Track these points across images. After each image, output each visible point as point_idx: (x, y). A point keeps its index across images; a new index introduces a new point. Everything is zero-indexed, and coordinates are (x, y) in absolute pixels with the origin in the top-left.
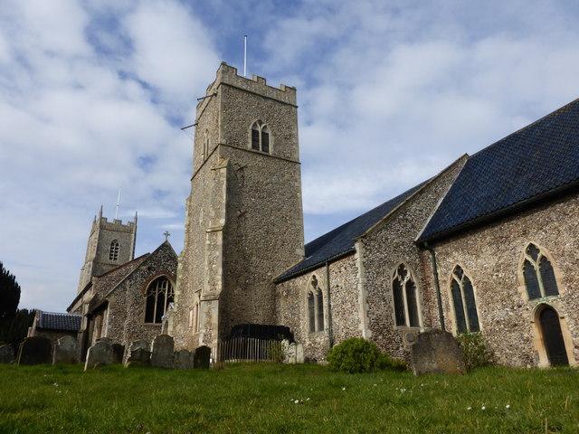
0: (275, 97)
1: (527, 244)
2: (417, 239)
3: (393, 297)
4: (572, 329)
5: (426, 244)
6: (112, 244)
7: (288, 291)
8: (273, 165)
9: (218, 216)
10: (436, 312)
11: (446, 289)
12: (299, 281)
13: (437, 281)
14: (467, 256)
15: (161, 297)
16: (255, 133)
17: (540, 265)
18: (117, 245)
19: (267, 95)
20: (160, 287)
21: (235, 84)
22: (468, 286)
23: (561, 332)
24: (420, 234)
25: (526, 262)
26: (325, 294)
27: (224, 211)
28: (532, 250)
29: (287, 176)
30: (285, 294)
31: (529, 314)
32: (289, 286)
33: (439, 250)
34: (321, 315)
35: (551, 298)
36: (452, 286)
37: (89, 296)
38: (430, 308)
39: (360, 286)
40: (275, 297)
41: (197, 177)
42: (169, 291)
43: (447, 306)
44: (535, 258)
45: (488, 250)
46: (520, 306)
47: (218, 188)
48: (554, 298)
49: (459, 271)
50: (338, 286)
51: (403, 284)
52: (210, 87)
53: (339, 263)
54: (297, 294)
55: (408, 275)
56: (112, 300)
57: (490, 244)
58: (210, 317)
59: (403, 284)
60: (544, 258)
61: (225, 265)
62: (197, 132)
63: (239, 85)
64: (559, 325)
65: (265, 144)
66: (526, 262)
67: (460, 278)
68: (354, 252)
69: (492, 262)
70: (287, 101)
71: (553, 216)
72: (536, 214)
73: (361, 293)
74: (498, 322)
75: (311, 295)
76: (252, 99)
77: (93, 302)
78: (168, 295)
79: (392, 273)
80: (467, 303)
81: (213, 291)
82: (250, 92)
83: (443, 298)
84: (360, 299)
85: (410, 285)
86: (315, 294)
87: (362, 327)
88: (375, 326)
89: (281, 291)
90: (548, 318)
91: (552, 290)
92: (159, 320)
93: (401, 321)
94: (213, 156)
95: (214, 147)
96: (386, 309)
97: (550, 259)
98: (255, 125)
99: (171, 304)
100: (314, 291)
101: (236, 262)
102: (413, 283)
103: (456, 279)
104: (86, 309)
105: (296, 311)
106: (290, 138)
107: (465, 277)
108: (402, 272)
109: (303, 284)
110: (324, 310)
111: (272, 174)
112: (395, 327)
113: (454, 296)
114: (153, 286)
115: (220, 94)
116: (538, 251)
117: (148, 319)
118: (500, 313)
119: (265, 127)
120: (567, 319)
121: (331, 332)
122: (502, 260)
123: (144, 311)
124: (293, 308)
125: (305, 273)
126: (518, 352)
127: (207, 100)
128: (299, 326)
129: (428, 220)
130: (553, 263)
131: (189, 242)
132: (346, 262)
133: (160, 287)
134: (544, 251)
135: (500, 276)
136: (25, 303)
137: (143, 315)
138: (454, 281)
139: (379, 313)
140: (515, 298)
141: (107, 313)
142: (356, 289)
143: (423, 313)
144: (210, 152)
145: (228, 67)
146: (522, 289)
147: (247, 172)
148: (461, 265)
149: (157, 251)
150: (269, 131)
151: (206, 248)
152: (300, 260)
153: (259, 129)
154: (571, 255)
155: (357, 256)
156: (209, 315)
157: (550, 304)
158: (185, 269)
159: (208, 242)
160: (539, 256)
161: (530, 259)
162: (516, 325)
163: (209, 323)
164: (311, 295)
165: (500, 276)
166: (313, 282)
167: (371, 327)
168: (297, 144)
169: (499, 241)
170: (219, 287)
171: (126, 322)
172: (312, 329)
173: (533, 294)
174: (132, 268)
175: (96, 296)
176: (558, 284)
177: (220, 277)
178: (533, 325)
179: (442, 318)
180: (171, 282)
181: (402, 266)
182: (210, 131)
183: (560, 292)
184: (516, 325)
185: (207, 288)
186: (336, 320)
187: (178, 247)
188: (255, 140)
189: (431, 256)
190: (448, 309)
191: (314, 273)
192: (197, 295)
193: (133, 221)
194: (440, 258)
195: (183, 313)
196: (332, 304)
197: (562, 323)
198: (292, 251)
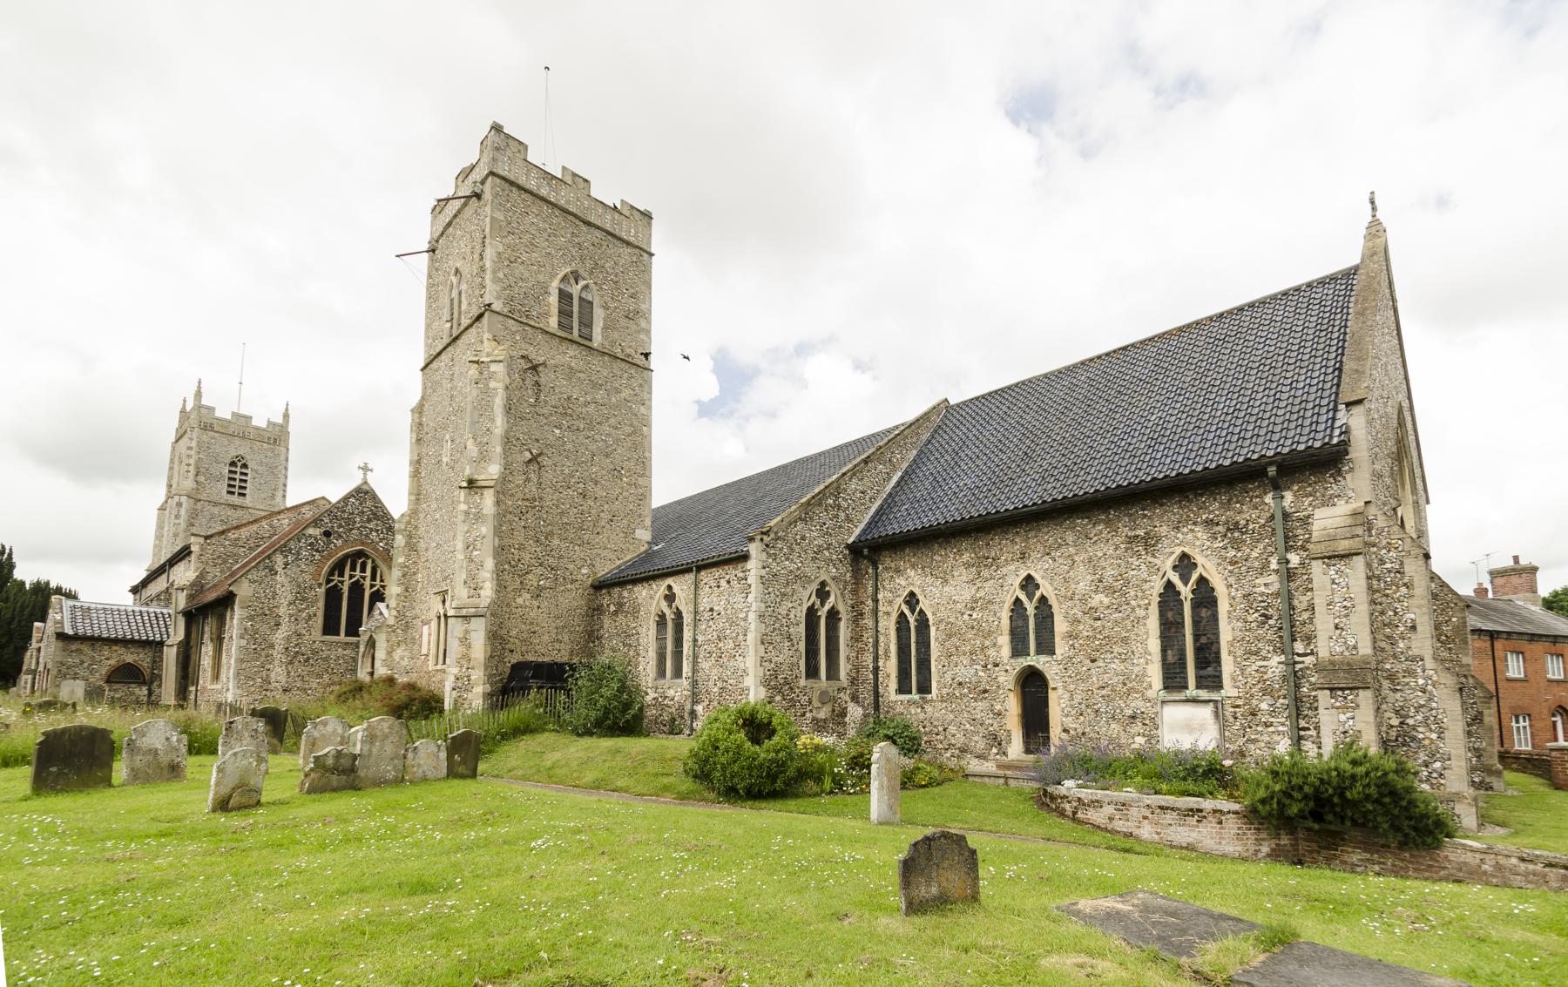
0: (608, 227)
1: (1023, 574)
2: (850, 541)
3: (804, 634)
4: (1064, 705)
5: (866, 551)
6: (233, 464)
7: (620, 605)
8: (599, 367)
9: (483, 457)
10: (868, 659)
11: (888, 626)
12: (642, 592)
13: (875, 612)
14: (929, 579)
15: (357, 588)
16: (565, 297)
17: (1036, 608)
18: (245, 466)
19: (592, 219)
20: (353, 569)
21: (522, 181)
22: (923, 624)
23: (1047, 706)
24: (857, 532)
25: (1018, 601)
26: (687, 618)
27: (499, 449)
28: (1029, 584)
29: (626, 393)
30: (612, 608)
31: (1007, 679)
32: (620, 596)
33: (887, 561)
34: (678, 654)
35: (1043, 658)
36: (898, 623)
37: (184, 574)
38: (861, 651)
39: (752, 616)
40: (595, 611)
41: (434, 365)
42: (373, 578)
43: (887, 652)
44: (1030, 596)
45: (962, 575)
46: (996, 665)
47: (483, 407)
48: (1048, 658)
49: (912, 600)
50: (712, 610)
51: (823, 613)
52: (466, 173)
53: (717, 572)
54: (635, 612)
55: (832, 599)
56: (243, 590)
57: (967, 565)
58: (469, 646)
59: (823, 613)
60: (1043, 599)
61: (500, 551)
62: (432, 260)
63: (532, 184)
64: (1046, 699)
65: (586, 323)
66: (1018, 601)
67: (913, 611)
68: (745, 557)
69: (967, 594)
70: (632, 239)
71: (1070, 537)
72: (1045, 530)
73: (752, 627)
74: (960, 684)
75: (662, 616)
76: (558, 219)
77: (197, 587)
78: (372, 586)
79: (806, 596)
80: (917, 650)
81: (475, 601)
82: (554, 205)
83: (882, 638)
84: (751, 637)
85: (833, 615)
86: (670, 616)
87: (750, 682)
88: (776, 683)
89: (605, 602)
90: (1033, 687)
91: (1046, 647)
92: (353, 630)
93: (812, 672)
94: (473, 330)
95: (475, 312)
96: (792, 655)
97: (1053, 601)
98: (564, 279)
99: (381, 606)
100: (667, 611)
101: (521, 548)
102: (838, 612)
103: (907, 612)
104: (181, 601)
105: (633, 641)
106: (636, 315)
107: (921, 610)
108: (822, 594)
109: (650, 598)
110: (685, 663)
111: (595, 386)
112: (803, 682)
113: (899, 638)
114: (339, 567)
115: (487, 196)
116: (1037, 586)
117: (330, 627)
118: (965, 672)
119: (586, 287)
120: (1060, 691)
121: (694, 684)
122: (981, 594)
123: (320, 614)
124: (628, 637)
125: (654, 578)
126: (982, 730)
127: (457, 204)
128: (637, 665)
129: (873, 509)
130: (1055, 609)
131: (417, 495)
132: (732, 572)
133: (353, 569)
134: (1046, 589)
135: (975, 616)
136: (18, 574)
137: (319, 621)
138: (902, 614)
139: (780, 659)
140: (992, 652)
141: (236, 620)
142: (745, 620)
143: (848, 658)
144: (465, 322)
145: (508, 136)
146: (1004, 640)
147: (545, 377)
148: (917, 591)
149: (346, 499)
150: (594, 297)
151: (461, 517)
152: (643, 549)
153: (575, 290)
154: (1083, 601)
155: (752, 565)
156: (465, 641)
157: (1039, 667)
158: (411, 547)
159: (463, 507)
160: (1038, 594)
161: (1023, 597)
162: (985, 691)
163: (466, 657)
164: (662, 616)
165: (975, 616)
166: (666, 597)
167: (766, 683)
168: (648, 332)
169: (980, 563)
170: (488, 592)
171: (280, 636)
172: (661, 673)
173: (1019, 649)
174: (285, 523)
175: (202, 575)
176: (1057, 639)
177: (488, 575)
178: (1012, 695)
179: (876, 670)
180: (379, 562)
181: (823, 584)
182: (465, 271)
183: (1058, 651)
184: (985, 691)
185: (461, 593)
186: (705, 665)
187: (396, 502)
188: (565, 313)
189: (870, 571)
190: (887, 657)
191: (670, 581)
192: (439, 598)
193: (280, 420)
194: (886, 575)
195: (407, 627)
196: (700, 638)
197: (1052, 696)
198: (629, 533)
